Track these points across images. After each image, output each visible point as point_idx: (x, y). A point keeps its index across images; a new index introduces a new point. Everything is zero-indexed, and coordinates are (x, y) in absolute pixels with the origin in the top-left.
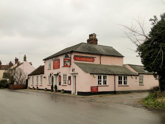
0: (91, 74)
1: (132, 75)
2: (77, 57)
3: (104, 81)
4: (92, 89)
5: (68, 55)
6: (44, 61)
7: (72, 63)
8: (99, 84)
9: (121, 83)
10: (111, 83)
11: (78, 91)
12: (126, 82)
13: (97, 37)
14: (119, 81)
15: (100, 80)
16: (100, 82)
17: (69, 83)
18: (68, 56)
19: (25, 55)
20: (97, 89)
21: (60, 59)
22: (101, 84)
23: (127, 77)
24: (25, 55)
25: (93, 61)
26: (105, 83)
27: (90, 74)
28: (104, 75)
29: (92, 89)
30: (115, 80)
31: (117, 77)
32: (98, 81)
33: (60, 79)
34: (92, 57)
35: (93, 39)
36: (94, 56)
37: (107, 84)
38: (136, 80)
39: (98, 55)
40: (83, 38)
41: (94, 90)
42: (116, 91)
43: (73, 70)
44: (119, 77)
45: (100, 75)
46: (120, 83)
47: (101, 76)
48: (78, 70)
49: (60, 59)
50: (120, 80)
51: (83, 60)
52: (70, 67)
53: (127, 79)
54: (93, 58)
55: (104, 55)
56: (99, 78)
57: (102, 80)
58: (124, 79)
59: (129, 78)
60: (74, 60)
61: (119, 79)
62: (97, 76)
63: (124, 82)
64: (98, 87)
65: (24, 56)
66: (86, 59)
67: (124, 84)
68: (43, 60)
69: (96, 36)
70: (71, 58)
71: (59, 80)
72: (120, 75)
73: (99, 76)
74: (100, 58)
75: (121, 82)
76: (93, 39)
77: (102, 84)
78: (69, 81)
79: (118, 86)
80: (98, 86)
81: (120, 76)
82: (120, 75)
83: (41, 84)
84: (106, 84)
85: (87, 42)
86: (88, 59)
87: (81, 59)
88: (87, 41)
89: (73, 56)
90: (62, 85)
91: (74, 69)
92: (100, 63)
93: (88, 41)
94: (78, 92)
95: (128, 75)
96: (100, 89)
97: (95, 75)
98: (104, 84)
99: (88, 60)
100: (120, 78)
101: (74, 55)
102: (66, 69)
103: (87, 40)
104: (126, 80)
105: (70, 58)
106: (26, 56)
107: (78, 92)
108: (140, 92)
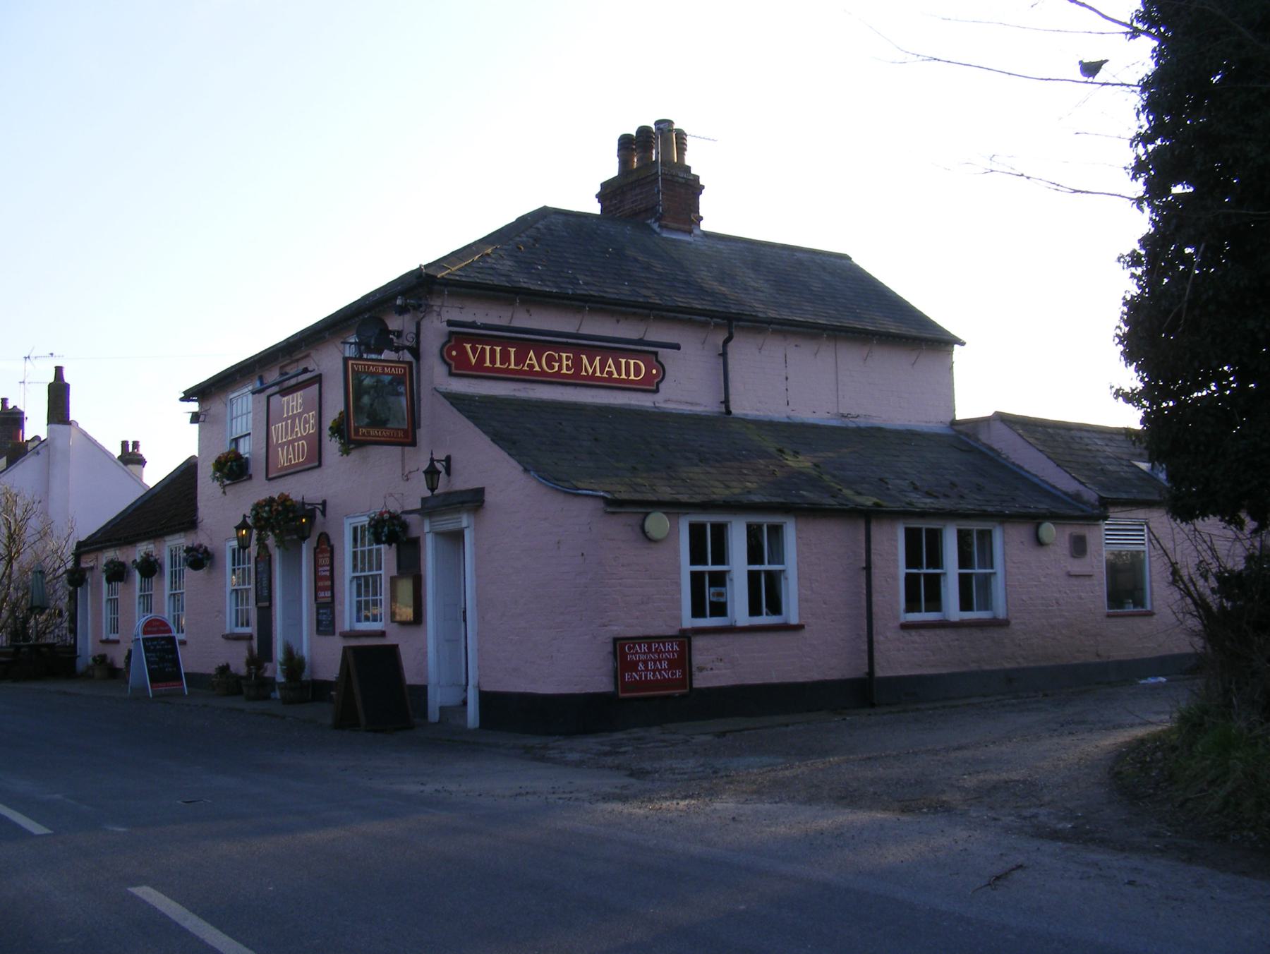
0: (614, 505)
1: (1035, 519)
2: (476, 339)
3: (753, 577)
4: (633, 666)
5: (394, 323)
6: (194, 406)
7: (430, 408)
8: (698, 611)
9: (935, 601)
10: (824, 596)
11: (487, 688)
12: (986, 581)
13: (689, 160)
14: (911, 581)
15: (710, 567)
16: (709, 593)
17: (407, 613)
18: (385, 331)
19: (59, 371)
20: (683, 661)
21: (320, 376)
22: (720, 609)
23: (990, 532)
24: (59, 371)
25: (651, 385)
26: (765, 593)
27: (601, 504)
28: (755, 519)
29: (633, 666)
30: (868, 568)
31: (892, 544)
32: (696, 578)
33: (323, 578)
34: (641, 342)
35: (653, 173)
36: (657, 333)
37: (791, 614)
38: (1077, 566)
39: (705, 325)
40: (576, 181)
41: (653, 669)
42: (879, 673)
43: (432, 473)
44: (912, 537)
45: (708, 519)
46: (923, 592)
47: (720, 532)
48: (481, 462)
49: (320, 376)
50: (919, 566)
51: (543, 373)
52: (408, 439)
53: (988, 561)
54: (647, 351)
55: (757, 325)
56: (709, 545)
57: (738, 564)
58: (965, 560)
59: (1007, 544)
60: (451, 374)
61: (912, 560)
62: (678, 534)
63: (964, 581)
64: (698, 643)
65: (52, 379)
66: (577, 364)
67: (966, 604)
68: (188, 396)
69: (682, 148)
70: (416, 352)
71: (317, 578)
72: (923, 514)
73: (697, 532)
74: (724, 355)
75: (934, 583)
76: (653, 173)
77: (739, 612)
78: (406, 587)
79: (906, 627)
80: (685, 637)
81: (923, 525)
82: (923, 514)
83: (115, 629)
84: (775, 608)
85: (595, 208)
86: (591, 366)
87: (520, 359)
88: (601, 197)
89: (434, 330)
90: (347, 628)
91: (448, 459)
92: (726, 402)
93: (608, 193)
94: (487, 699)
95: (1003, 518)
96: (717, 666)
97: (657, 523)
98: (754, 610)
99: (593, 377)
100: (923, 549)
101: (450, 323)
102: (384, 460)
103: (598, 189)
104: (977, 571)
105: (408, 357)
106: (67, 380)
107: (487, 699)
108: (265, 592)
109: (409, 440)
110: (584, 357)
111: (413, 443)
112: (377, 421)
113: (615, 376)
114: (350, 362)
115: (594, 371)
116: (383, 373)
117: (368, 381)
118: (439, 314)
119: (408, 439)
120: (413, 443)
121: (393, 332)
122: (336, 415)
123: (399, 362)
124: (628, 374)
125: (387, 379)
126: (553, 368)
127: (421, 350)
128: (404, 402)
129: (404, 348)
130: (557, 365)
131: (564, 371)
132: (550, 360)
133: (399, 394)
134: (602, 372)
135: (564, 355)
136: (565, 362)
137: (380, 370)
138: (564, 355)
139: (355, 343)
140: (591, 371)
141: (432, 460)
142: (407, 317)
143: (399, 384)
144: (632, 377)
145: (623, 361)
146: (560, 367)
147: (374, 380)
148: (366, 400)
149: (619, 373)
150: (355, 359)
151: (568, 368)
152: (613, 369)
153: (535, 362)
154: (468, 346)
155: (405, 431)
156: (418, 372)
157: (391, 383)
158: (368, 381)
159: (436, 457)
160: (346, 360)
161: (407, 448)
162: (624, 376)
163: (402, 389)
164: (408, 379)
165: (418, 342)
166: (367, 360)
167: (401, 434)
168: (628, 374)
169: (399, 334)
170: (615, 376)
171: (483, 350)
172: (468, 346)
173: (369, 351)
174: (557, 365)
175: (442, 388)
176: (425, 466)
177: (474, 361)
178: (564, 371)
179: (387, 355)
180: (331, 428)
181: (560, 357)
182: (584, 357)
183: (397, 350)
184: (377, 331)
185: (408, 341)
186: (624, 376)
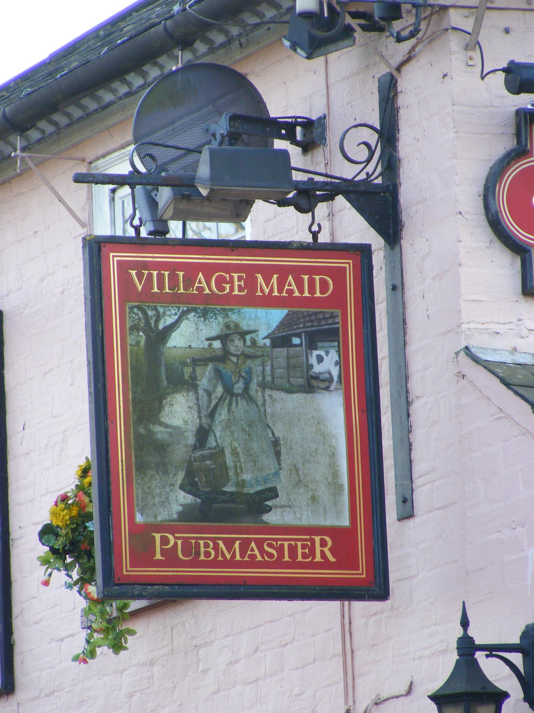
18: (256, 124)
52: (356, 570)
70: (382, 205)
105: (347, 224)
109: (361, 573)
110: (259, 276)
111: (377, 588)
112: (226, 503)
113: (297, 294)
114: (114, 258)
115: (272, 291)
116: (252, 300)
117: (188, 336)
118: (473, 44)
119: (356, 570)
120: (377, 588)
121: (286, 128)
122: (67, 481)
123: (314, 248)
124: (312, 290)
125: (265, 321)
126: (224, 289)
127: (407, 194)
128: (332, 409)
129: (333, 189)
130: (228, 286)
131: (236, 292)
132: (220, 281)
133: (312, 384)
134: (280, 291)
135: (236, 276)
136: (236, 283)
137: (236, 285)
138: (236, 276)
139: (131, 180)
140: (267, 291)
141: (467, 647)
142: (342, 61)
143: (313, 341)
144: (318, 294)
145: (306, 277)
146: (232, 289)
147: (214, 327)
148: (180, 412)
149: (301, 291)
150: (136, 243)
151: (240, 289)
152: (294, 287)
153: (204, 284)
154: (133, 273)
155: (342, 538)
156: (397, 288)
157: (280, 339)
158: (188, 336)
159: (480, 635)
160: (97, 249)
161: (358, 606)
162: (306, 294)
163: (326, 362)
164: (341, 316)
165: (391, 165)
166: (185, 244)
167: (324, 550)
168: (312, 290)
169: (311, 133)
170: (297, 294)
171: (150, 276)
172: (133, 273)
173: (189, 200)
174: (228, 286)
175: (498, 351)
176: (440, 669)
177: (140, 288)
178: (236, 292)
179: (268, 221)
180: (47, 532)
181: (232, 278)
182: (259, 276)
183: (306, 198)
184: (222, 126)
185: (347, 158)
186: (306, 294)
